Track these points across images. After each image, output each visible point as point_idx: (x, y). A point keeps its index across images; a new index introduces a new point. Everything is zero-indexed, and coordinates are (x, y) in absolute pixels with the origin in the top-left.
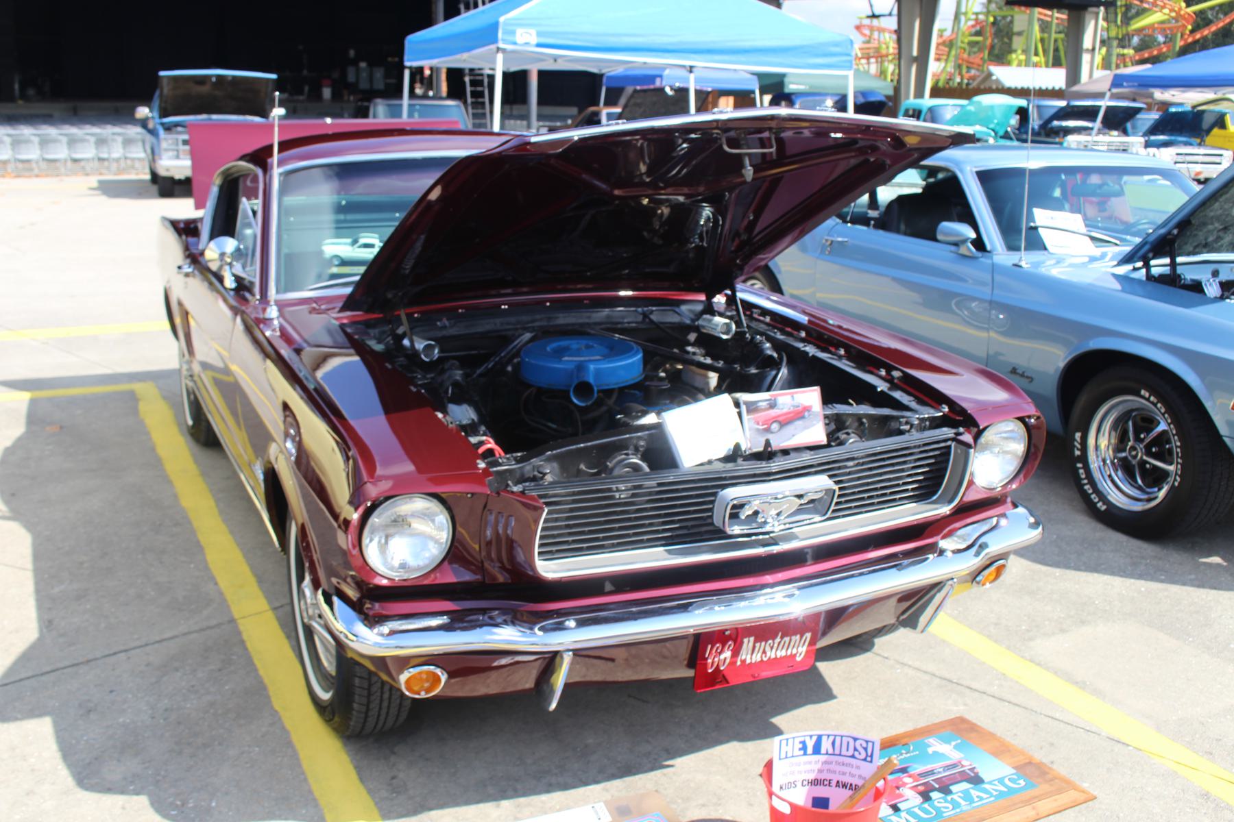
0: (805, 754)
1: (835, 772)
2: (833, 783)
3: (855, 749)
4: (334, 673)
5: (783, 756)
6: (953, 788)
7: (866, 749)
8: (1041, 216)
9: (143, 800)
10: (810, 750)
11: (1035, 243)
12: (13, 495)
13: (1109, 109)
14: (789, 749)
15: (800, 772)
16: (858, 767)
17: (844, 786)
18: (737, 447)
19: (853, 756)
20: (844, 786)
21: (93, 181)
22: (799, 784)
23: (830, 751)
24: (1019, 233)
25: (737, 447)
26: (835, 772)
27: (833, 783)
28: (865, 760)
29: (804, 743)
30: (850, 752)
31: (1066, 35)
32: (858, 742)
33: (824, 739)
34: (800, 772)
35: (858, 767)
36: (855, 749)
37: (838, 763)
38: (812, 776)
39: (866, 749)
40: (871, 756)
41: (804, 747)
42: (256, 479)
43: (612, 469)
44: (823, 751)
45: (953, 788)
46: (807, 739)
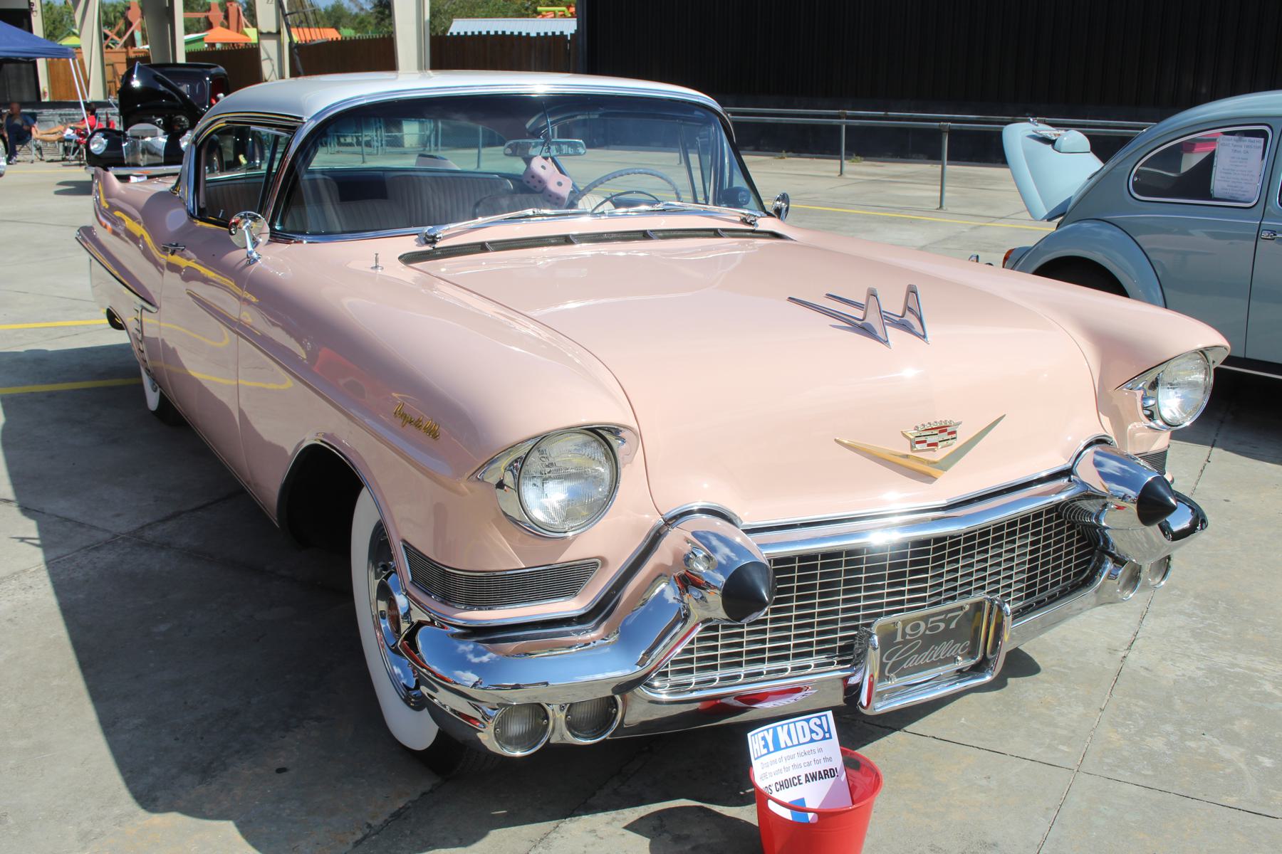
3: (812, 731)
6: (98, 111)
9: (228, 829)
10: (771, 749)
16: (820, 750)
17: (814, 777)
18: (802, 800)
19: (812, 740)
20: (814, 777)
23: (789, 744)
25: (802, 800)
27: (803, 780)
28: (824, 738)
30: (808, 739)
31: (693, 146)
32: (821, 736)
36: (812, 731)
39: (821, 726)
41: (766, 746)
42: (1042, 620)
43: (214, 253)
44: (783, 745)
45: (98, 111)
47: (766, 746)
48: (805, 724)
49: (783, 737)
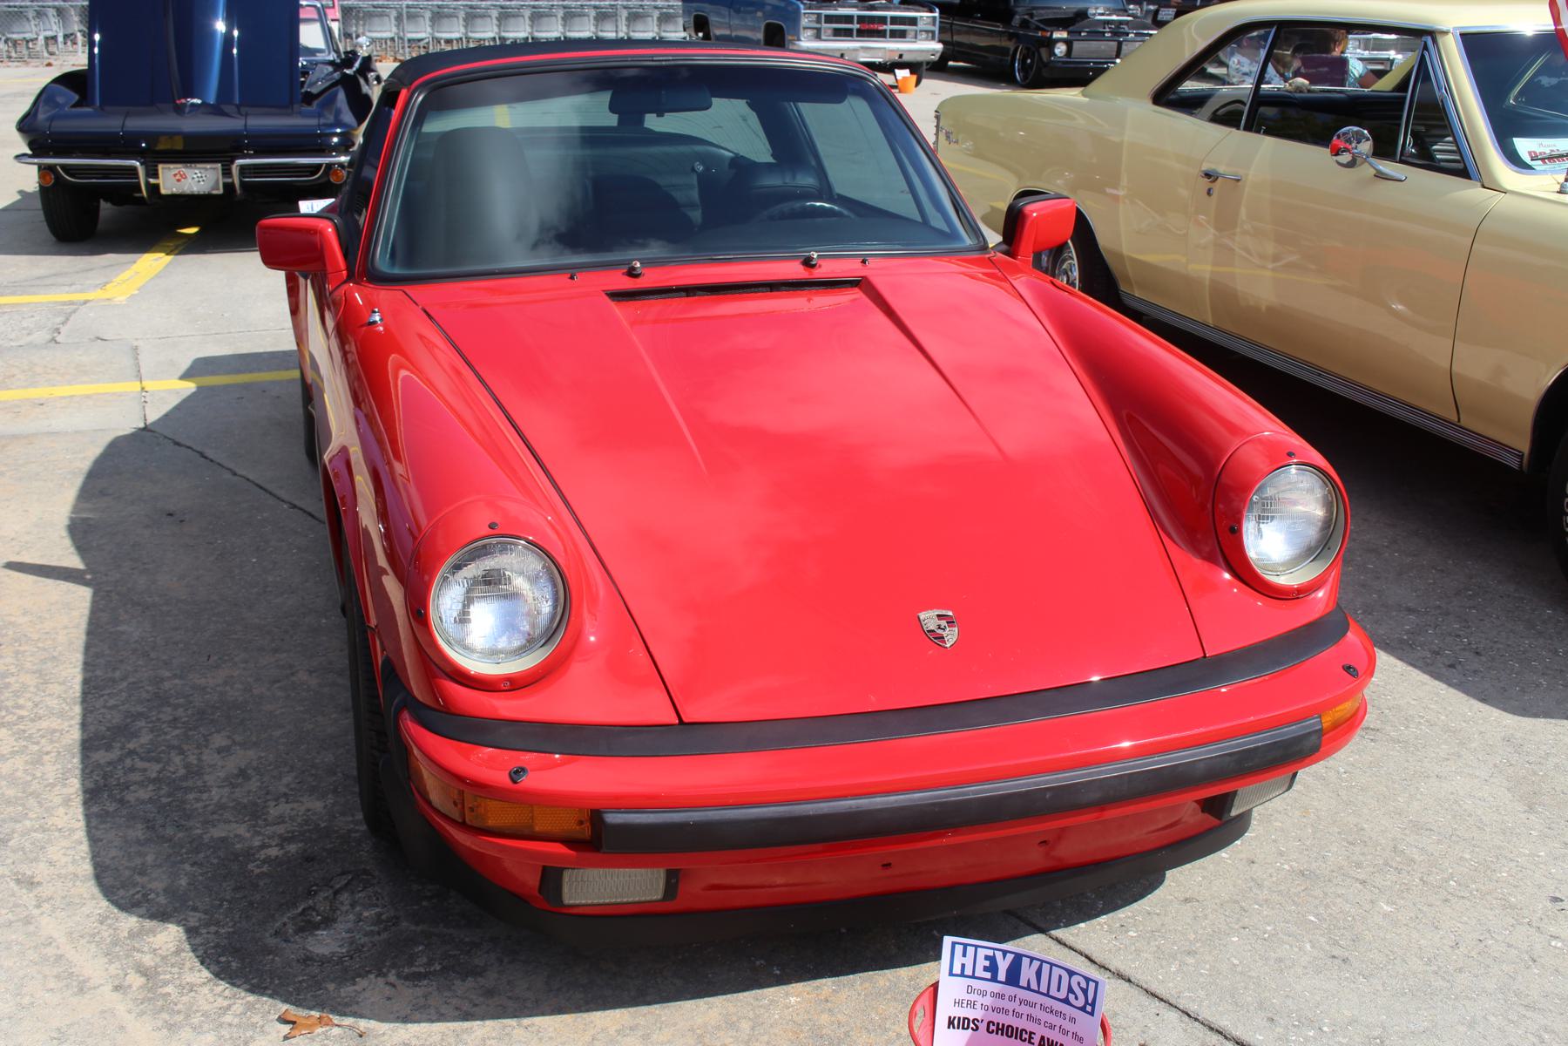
0: (994, 979)
3: (1070, 990)
5: (957, 970)
7: (1085, 991)
10: (1002, 976)
14: (969, 961)
16: (1073, 1020)
19: (1066, 1001)
28: (1083, 1009)
29: (992, 959)
30: (1063, 994)
33: (1025, 961)
35: (1073, 1020)
36: (1070, 990)
39: (1085, 991)
40: (1093, 1004)
41: (992, 968)
44: (1023, 983)
46: (999, 955)
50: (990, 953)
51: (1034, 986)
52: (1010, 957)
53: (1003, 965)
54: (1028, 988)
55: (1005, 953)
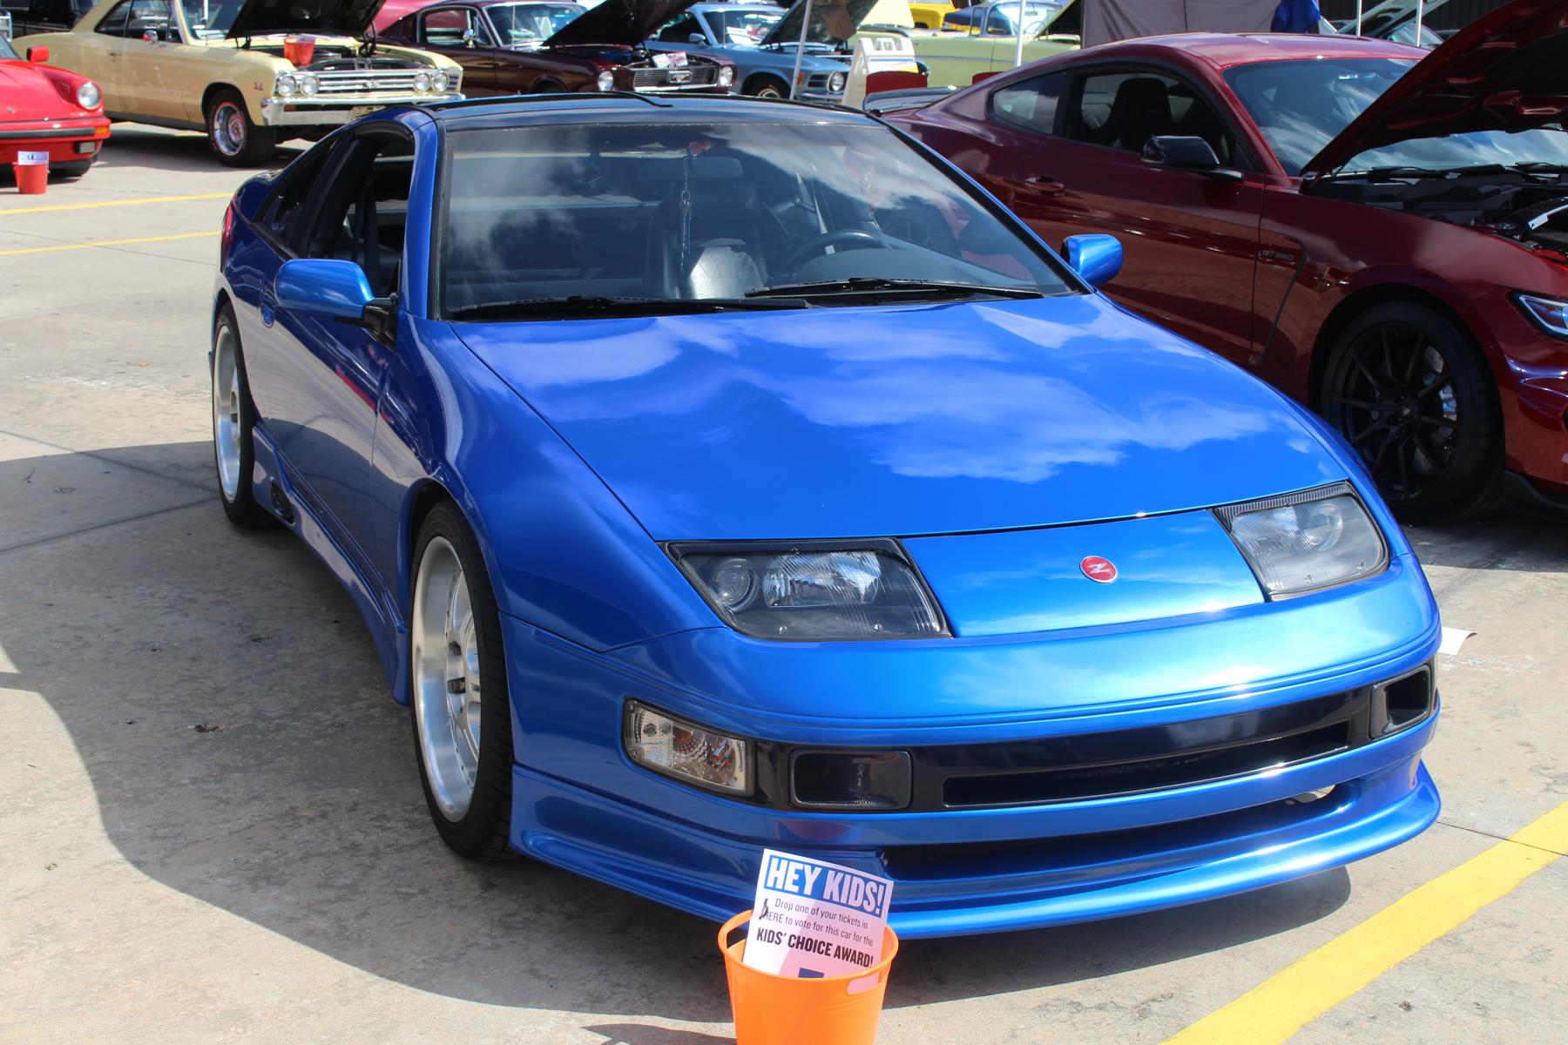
0: (801, 893)
1: (835, 932)
2: (832, 951)
3: (865, 897)
4: (230, 499)
5: (770, 884)
7: (876, 895)
8: (730, 30)
10: (808, 890)
11: (728, 40)
12: (257, 640)
13: (797, 39)
15: (789, 921)
16: (865, 925)
19: (861, 908)
21: (825, 978)
22: (785, 940)
24: (721, 36)
26: (835, 932)
27: (832, 951)
28: (873, 913)
29: (801, 873)
30: (857, 904)
33: (831, 874)
34: (789, 921)
36: (865, 897)
37: (842, 918)
38: (796, 930)
39: (876, 895)
41: (801, 882)
44: (826, 895)
47: (801, 882)
48: (861, 882)
49: (831, 886)
50: (800, 867)
51: (836, 898)
52: (818, 871)
53: (811, 878)
54: (831, 901)
55: (813, 866)
